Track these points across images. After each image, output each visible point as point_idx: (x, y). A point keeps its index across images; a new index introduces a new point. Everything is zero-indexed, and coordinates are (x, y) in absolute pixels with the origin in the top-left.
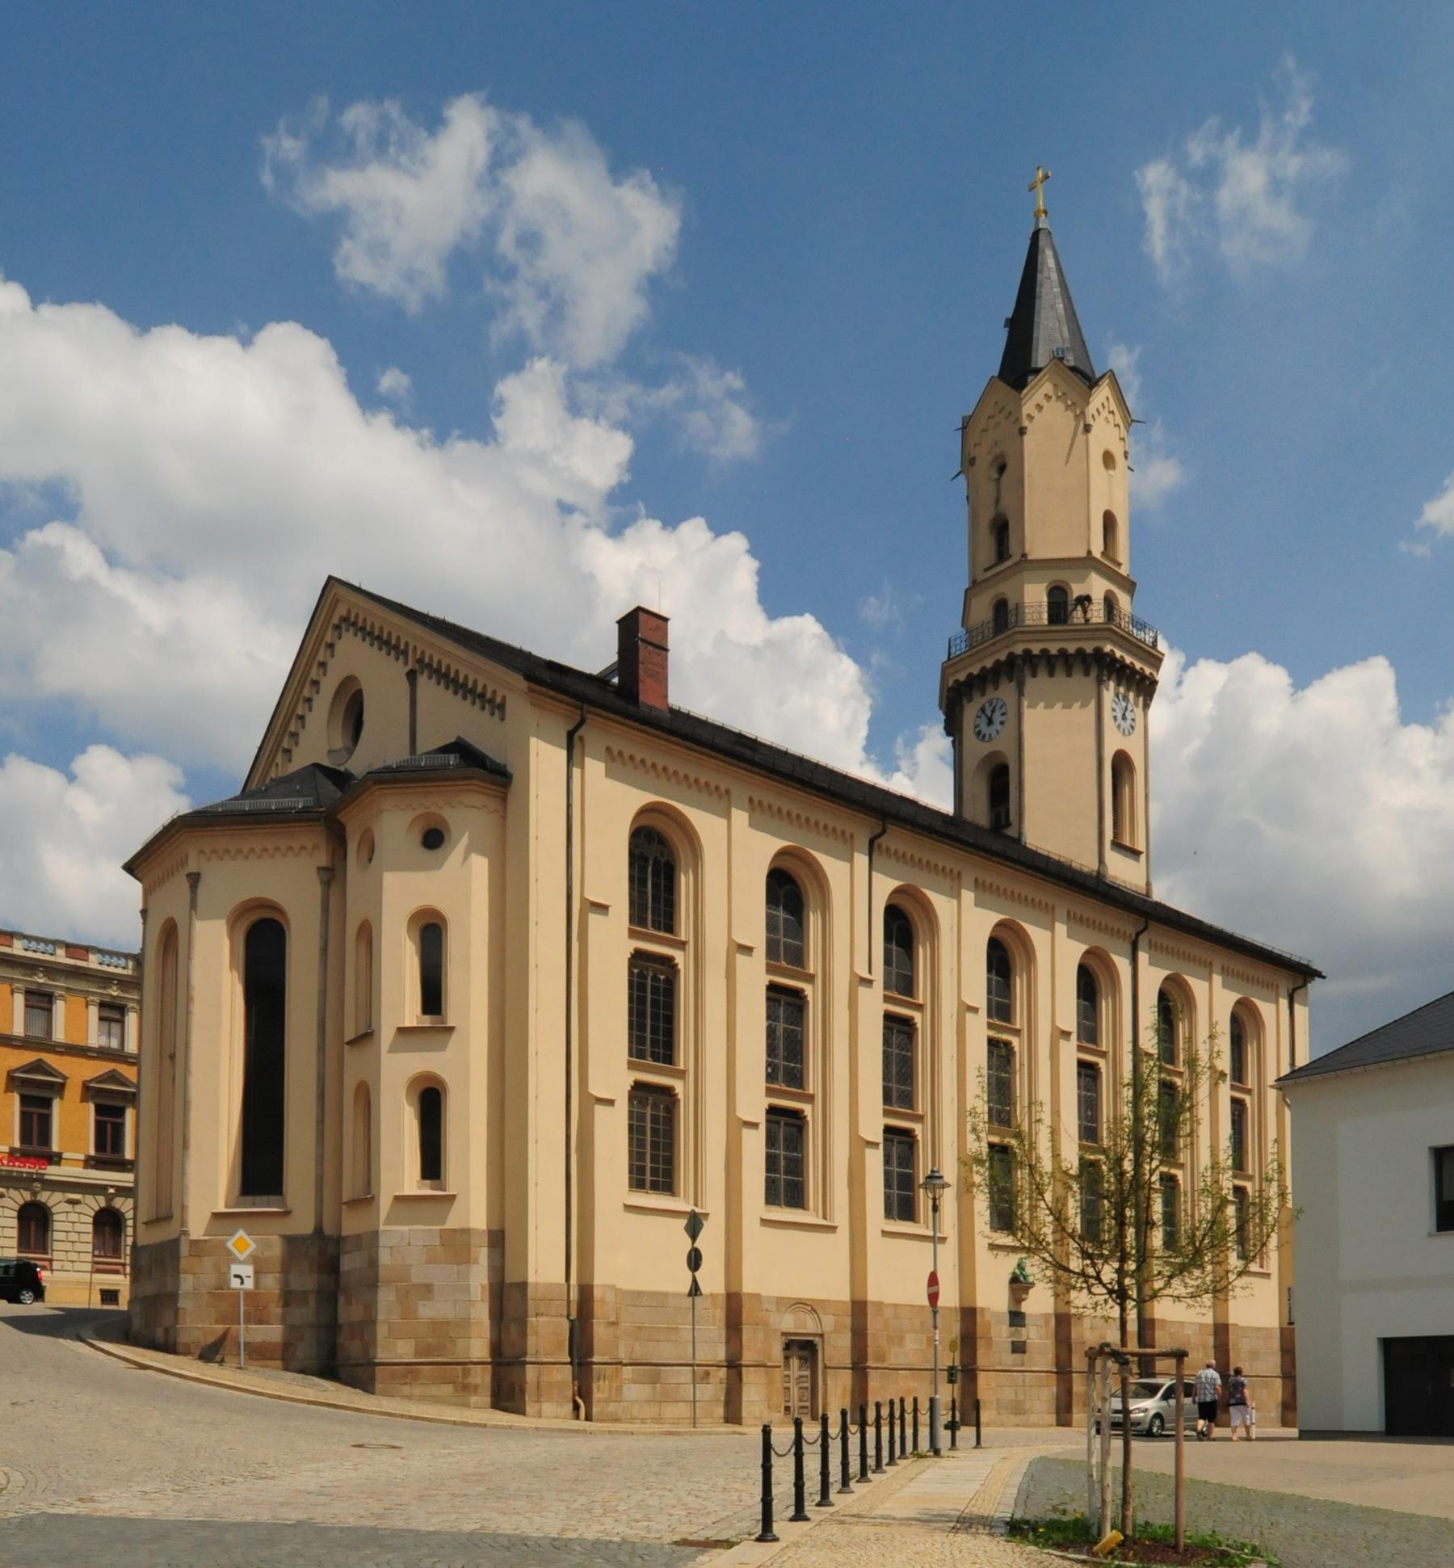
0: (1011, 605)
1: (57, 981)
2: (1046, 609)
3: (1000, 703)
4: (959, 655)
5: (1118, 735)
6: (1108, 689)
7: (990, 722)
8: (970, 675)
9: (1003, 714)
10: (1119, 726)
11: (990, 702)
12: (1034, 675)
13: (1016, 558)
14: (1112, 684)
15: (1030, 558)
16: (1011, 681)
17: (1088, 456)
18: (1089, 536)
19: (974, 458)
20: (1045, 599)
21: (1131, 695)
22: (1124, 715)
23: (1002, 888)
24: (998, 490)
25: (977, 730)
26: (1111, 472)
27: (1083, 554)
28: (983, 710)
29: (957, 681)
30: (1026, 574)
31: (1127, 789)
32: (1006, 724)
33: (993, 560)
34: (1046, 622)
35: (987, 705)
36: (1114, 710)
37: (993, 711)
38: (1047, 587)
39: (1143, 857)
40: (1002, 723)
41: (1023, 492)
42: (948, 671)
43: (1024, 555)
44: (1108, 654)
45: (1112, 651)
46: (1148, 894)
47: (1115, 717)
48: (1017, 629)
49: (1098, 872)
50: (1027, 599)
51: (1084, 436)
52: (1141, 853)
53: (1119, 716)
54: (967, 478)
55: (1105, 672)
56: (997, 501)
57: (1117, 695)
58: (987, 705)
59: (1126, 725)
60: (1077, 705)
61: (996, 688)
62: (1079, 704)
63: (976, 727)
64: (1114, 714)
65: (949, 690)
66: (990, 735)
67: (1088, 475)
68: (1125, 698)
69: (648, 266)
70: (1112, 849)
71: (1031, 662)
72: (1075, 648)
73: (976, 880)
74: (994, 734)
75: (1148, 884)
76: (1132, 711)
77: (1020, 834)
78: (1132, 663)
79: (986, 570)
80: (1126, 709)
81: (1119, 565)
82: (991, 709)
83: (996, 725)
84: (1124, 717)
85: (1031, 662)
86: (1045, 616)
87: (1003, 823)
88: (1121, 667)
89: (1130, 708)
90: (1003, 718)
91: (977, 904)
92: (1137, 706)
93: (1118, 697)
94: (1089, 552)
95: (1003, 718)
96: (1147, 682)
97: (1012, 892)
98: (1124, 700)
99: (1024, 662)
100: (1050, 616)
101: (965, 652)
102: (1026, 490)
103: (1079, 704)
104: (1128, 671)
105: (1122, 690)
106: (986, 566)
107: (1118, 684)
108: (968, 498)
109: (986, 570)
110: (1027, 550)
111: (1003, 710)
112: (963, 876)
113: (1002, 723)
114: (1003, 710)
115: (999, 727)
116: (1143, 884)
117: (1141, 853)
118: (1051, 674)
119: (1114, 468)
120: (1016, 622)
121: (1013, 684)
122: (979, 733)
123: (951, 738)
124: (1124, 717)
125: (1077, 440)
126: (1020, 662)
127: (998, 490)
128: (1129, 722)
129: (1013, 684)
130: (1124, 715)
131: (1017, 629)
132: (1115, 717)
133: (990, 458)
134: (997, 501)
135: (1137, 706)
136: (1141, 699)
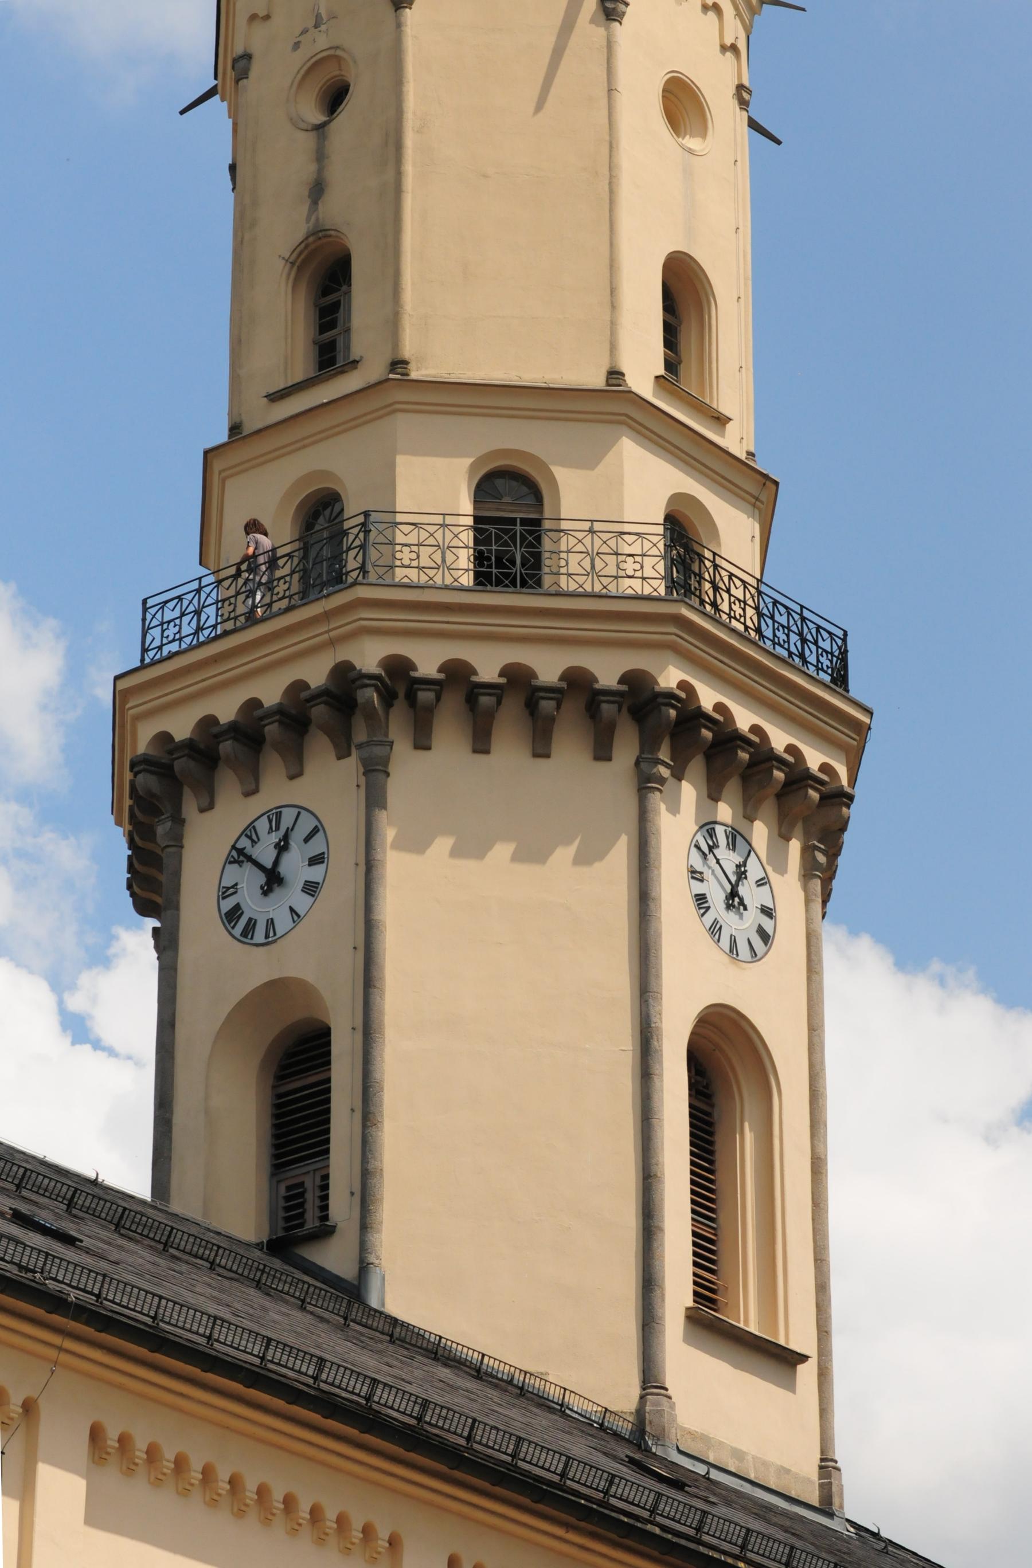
0: (352, 507)
1: (750, 1131)
2: (468, 537)
3: (306, 824)
4: (172, 656)
5: (715, 956)
6: (674, 809)
7: (273, 879)
8: (208, 722)
9: (316, 860)
10: (715, 930)
11: (275, 817)
12: (422, 743)
13: (372, 371)
14: (689, 792)
15: (414, 375)
16: (343, 754)
17: (611, 90)
18: (613, 325)
19: (247, 57)
20: (466, 506)
21: (760, 833)
22: (733, 894)
23: (196, 1466)
24: (321, 156)
25: (227, 905)
26: (692, 143)
27: (597, 380)
28: (250, 832)
29: (164, 738)
30: (404, 425)
31: (748, 1141)
32: (324, 893)
33: (301, 368)
34: (467, 580)
35: (263, 826)
36: (695, 875)
37: (282, 847)
38: (473, 467)
39: (806, 1373)
40: (311, 888)
41: (399, 174)
42: (135, 705)
43: (398, 364)
44: (670, 695)
45: (683, 685)
46: (826, 1508)
47: (701, 899)
48: (362, 592)
49: (640, 1413)
50: (402, 502)
51: (601, 31)
52: (803, 1358)
53: (717, 897)
54: (234, 113)
55: (664, 754)
56: (317, 190)
57: (708, 828)
58: (263, 826)
59: (734, 924)
60: (564, 855)
61: (295, 775)
62: (572, 850)
63: (226, 892)
64: (698, 888)
65: (139, 764)
66: (271, 922)
67: (612, 146)
68: (735, 837)
69: (682, 365)
70: (687, 1339)
71: (411, 698)
72: (559, 672)
73: (96, 1434)
74: (282, 923)
75: (827, 1467)
76: (761, 883)
77: (364, 1268)
78: (719, 707)
79: (276, 397)
80: (741, 873)
81: (721, 420)
82: (275, 838)
83: (293, 896)
84: (734, 900)
85: (411, 698)
86: (464, 559)
87: (311, 1221)
88: (681, 721)
89: (754, 870)
90: (315, 873)
91: (92, 1519)
92: (782, 870)
93: (712, 833)
94: (615, 375)
95: (315, 873)
96: (814, 795)
97: (234, 1482)
98: (732, 846)
99: (388, 698)
100: (480, 558)
101: (191, 648)
102: (409, 168)
103: (572, 850)
104: (744, 756)
105: (725, 812)
106: (280, 384)
107: (714, 795)
108: (233, 168)
109: (276, 397)
110: (408, 350)
111: (317, 846)
112: (45, 1410)
113: (311, 888)
114: (317, 846)
115: (302, 902)
116: (811, 1471)
117: (803, 1358)
118: (541, 749)
119: (702, 129)
120: (363, 569)
121: (352, 764)
122: (233, 915)
123: (152, 923)
124: (734, 900)
125: (575, 40)
126: (371, 695)
127: (321, 156)
128: (752, 917)
129: (352, 764)
130: (733, 894)
131: (362, 592)
132: (701, 899)
133: (298, 60)
134: (317, 190)
135: (782, 870)
136: (795, 846)
